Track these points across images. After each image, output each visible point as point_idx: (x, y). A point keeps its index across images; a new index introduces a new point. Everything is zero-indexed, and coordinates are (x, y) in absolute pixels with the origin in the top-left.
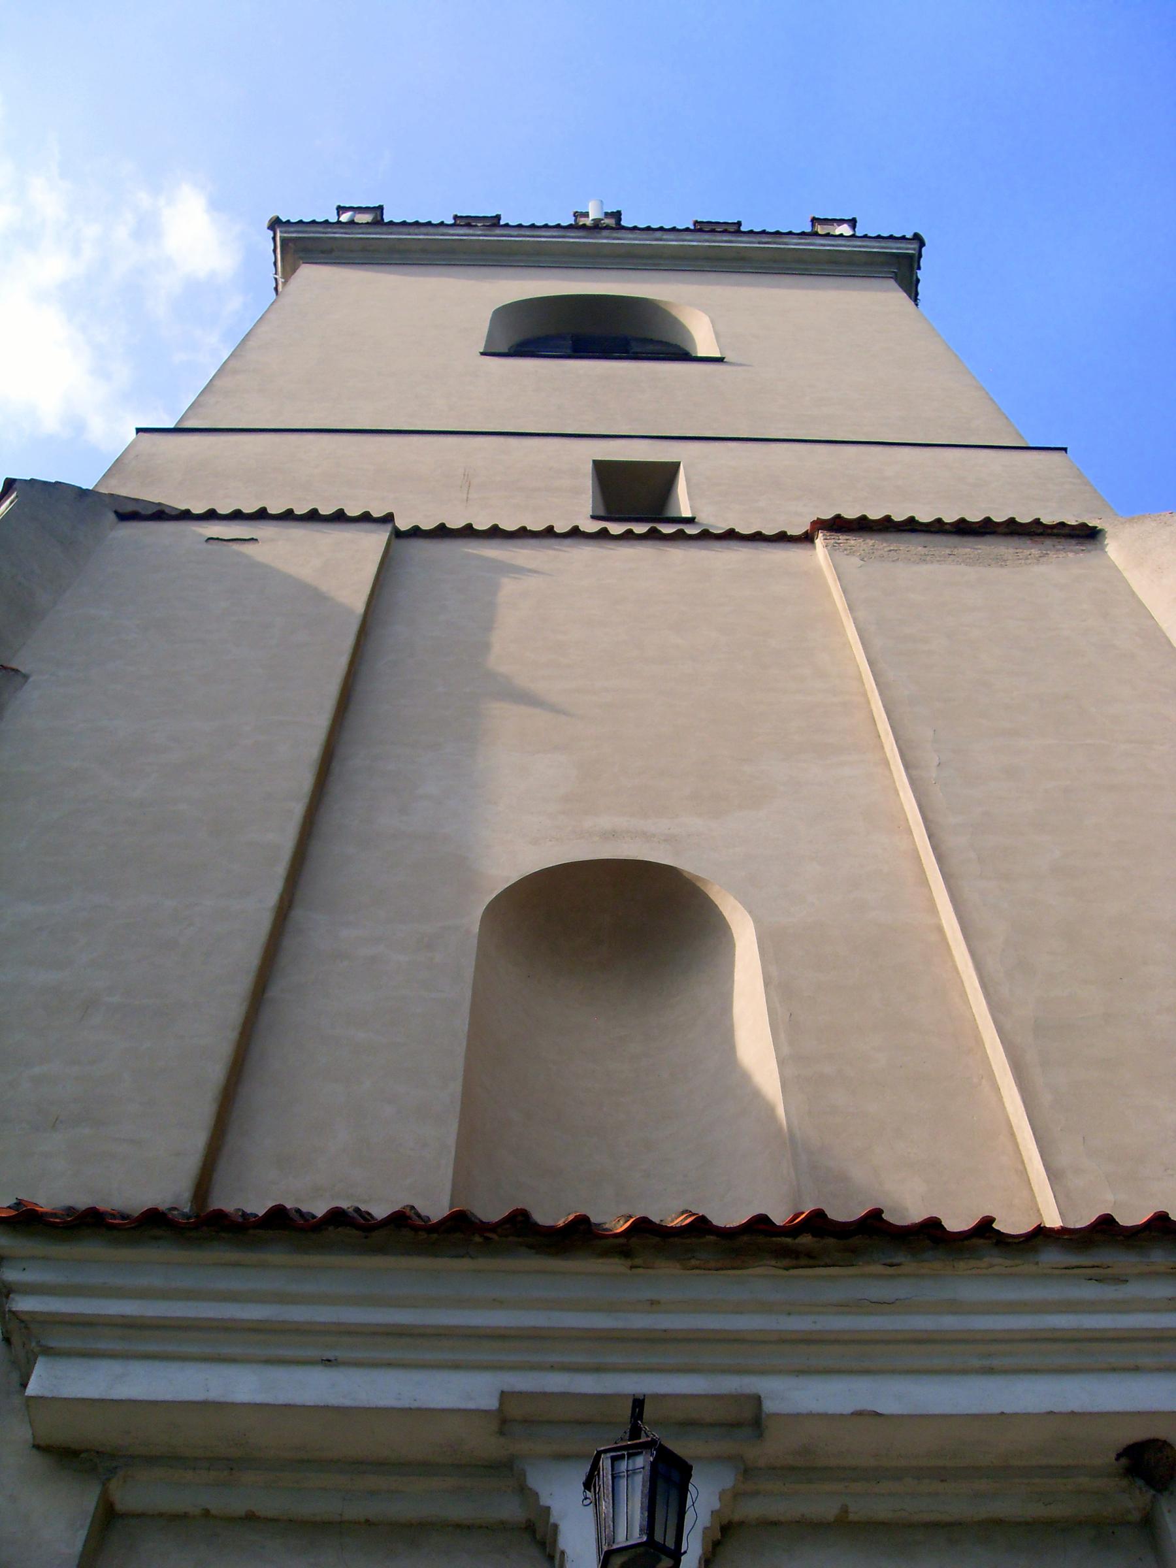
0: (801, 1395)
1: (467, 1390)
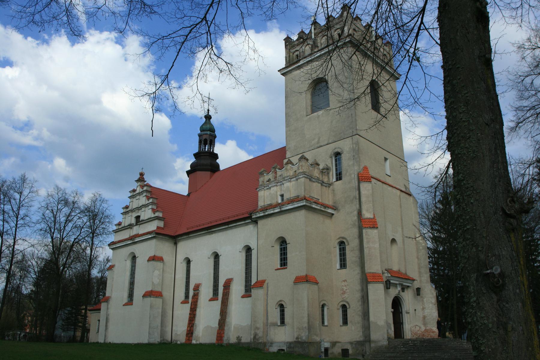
0: (404, 284)
1: (397, 282)
